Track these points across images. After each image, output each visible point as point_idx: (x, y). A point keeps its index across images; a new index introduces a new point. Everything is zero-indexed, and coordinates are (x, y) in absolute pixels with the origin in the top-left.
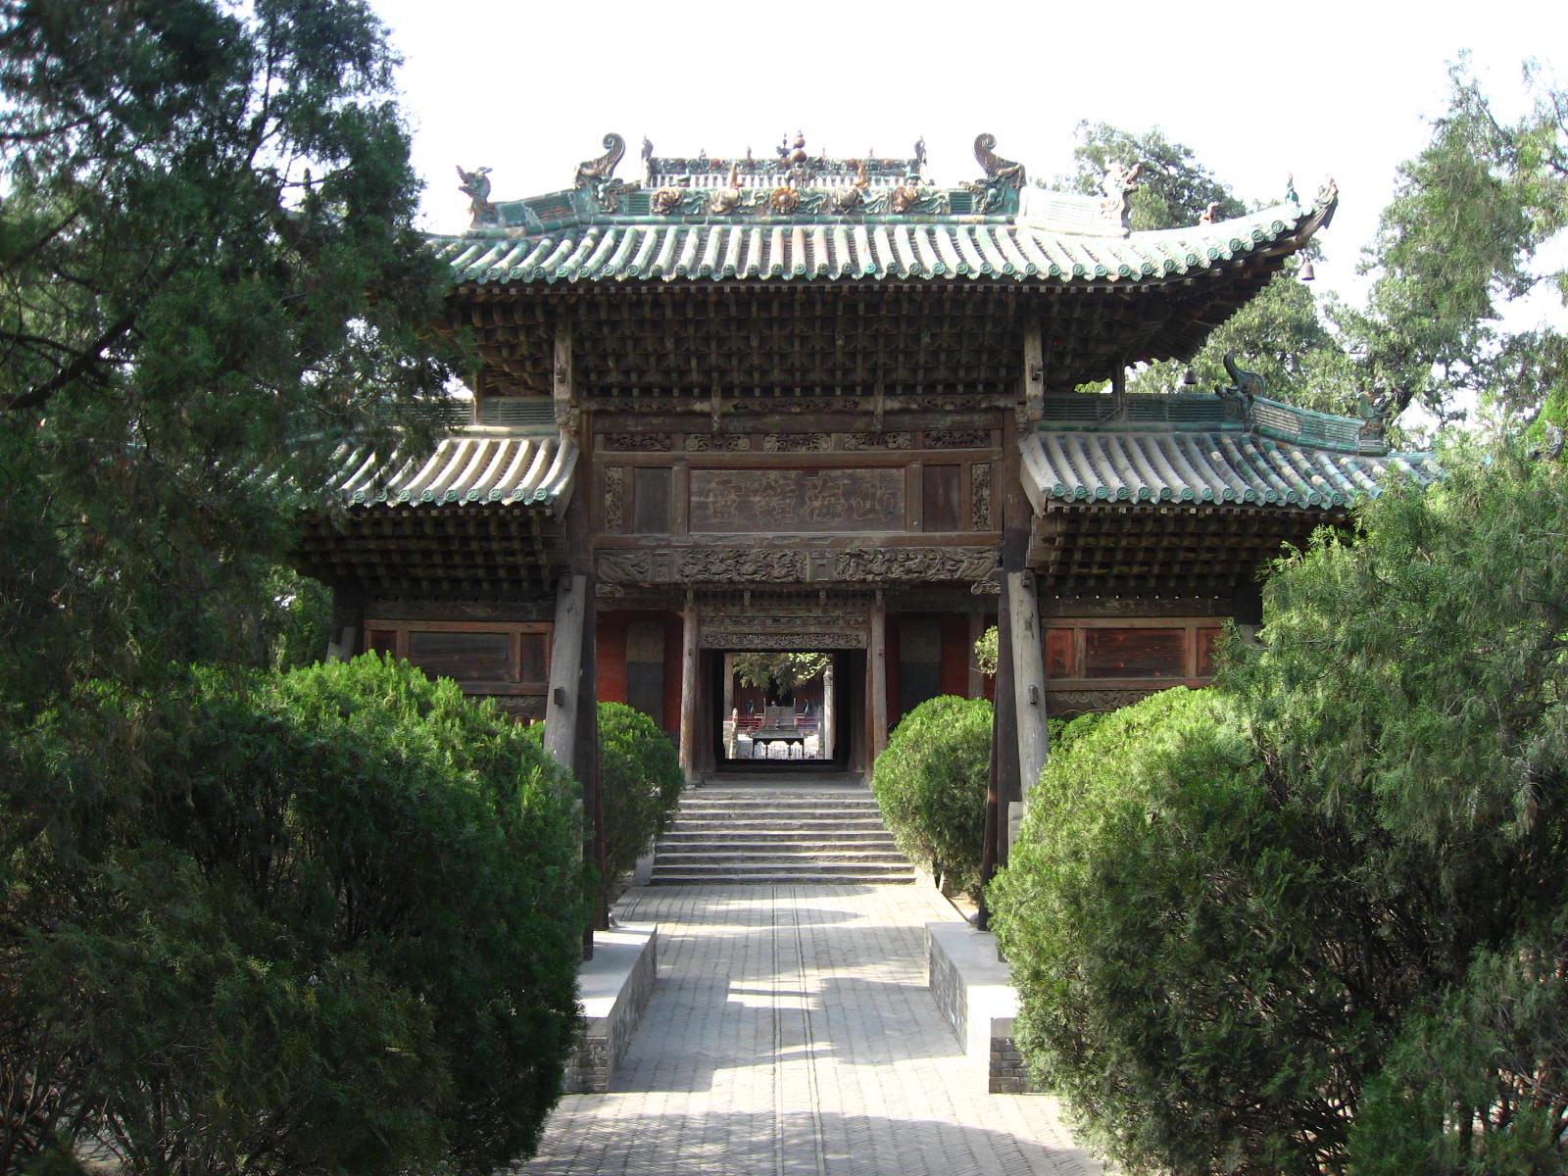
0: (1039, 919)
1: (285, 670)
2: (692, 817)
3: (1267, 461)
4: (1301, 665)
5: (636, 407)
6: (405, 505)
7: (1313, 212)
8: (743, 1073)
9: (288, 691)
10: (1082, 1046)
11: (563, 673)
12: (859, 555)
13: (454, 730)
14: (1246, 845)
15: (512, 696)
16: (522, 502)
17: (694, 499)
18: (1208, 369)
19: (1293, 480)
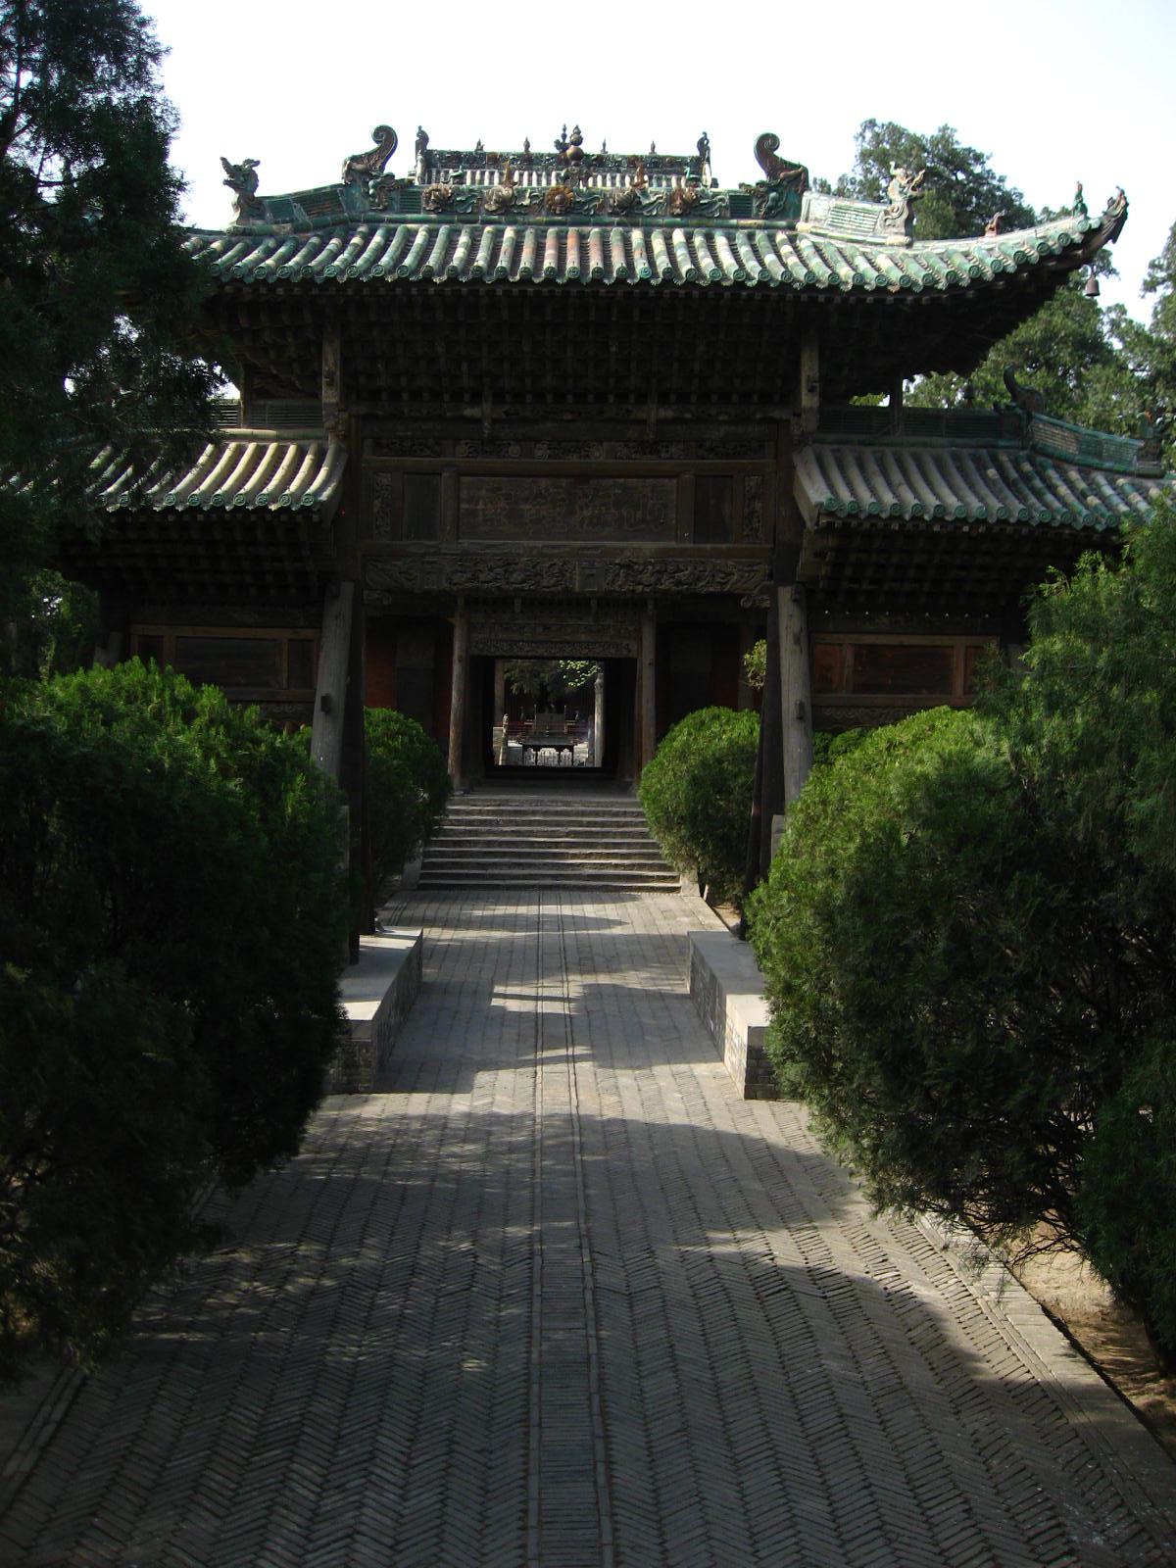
0: (794, 934)
1: (51, 677)
2: (459, 823)
3: (1044, 480)
4: (1062, 691)
5: (406, 411)
6: (170, 510)
7: (1101, 225)
8: (505, 1077)
9: (51, 699)
10: (832, 1058)
11: (329, 681)
12: (628, 566)
13: (219, 737)
14: (998, 869)
15: (278, 703)
16: (289, 508)
17: (464, 506)
18: (988, 384)
19: (1068, 499)
